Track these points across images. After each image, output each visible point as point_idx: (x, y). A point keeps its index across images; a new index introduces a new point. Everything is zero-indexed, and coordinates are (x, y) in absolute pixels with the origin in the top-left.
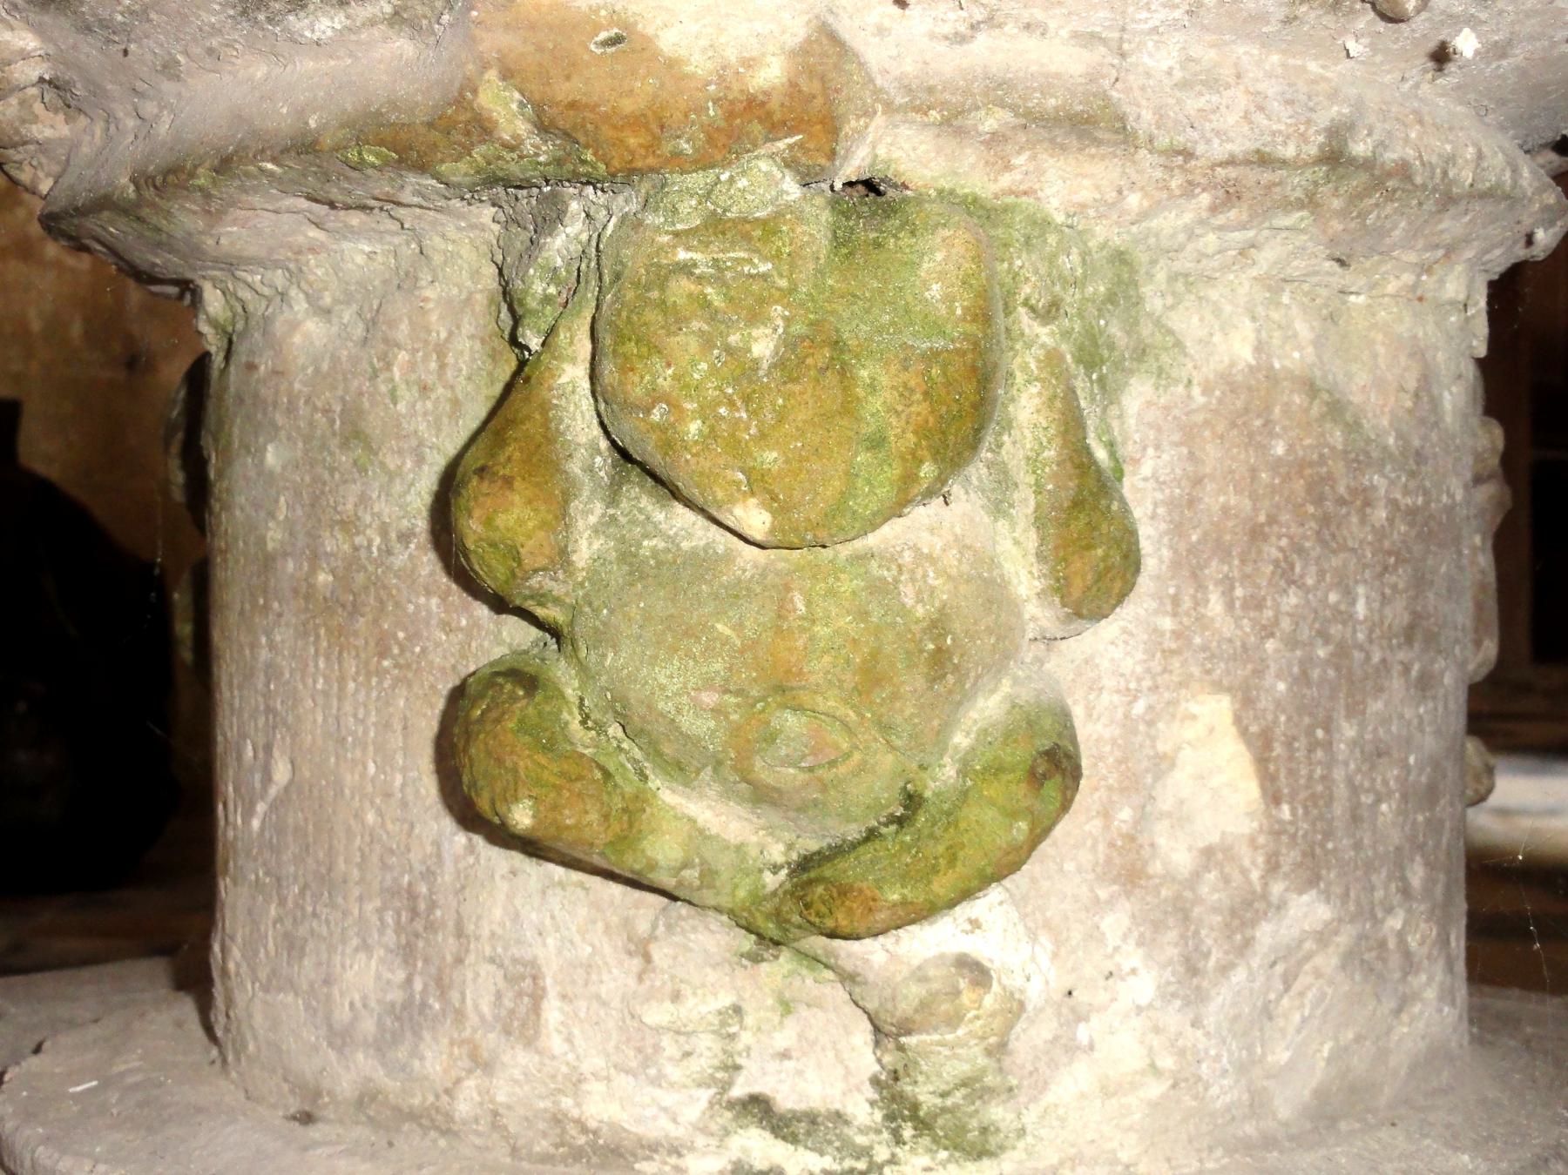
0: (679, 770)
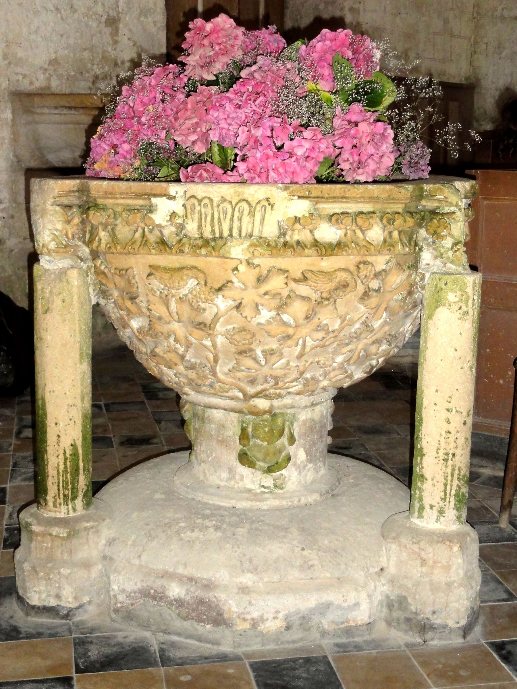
0: (258, 461)
